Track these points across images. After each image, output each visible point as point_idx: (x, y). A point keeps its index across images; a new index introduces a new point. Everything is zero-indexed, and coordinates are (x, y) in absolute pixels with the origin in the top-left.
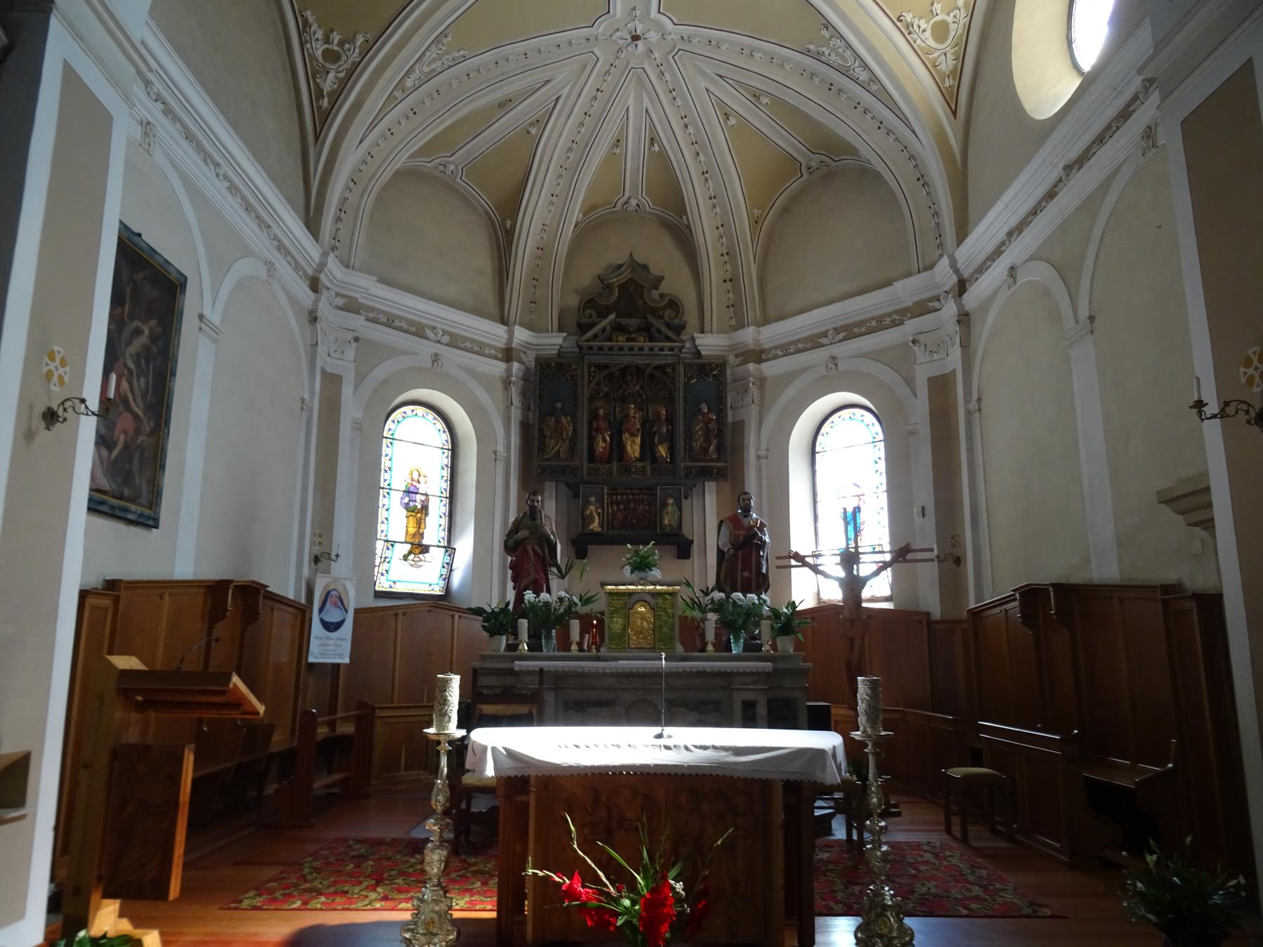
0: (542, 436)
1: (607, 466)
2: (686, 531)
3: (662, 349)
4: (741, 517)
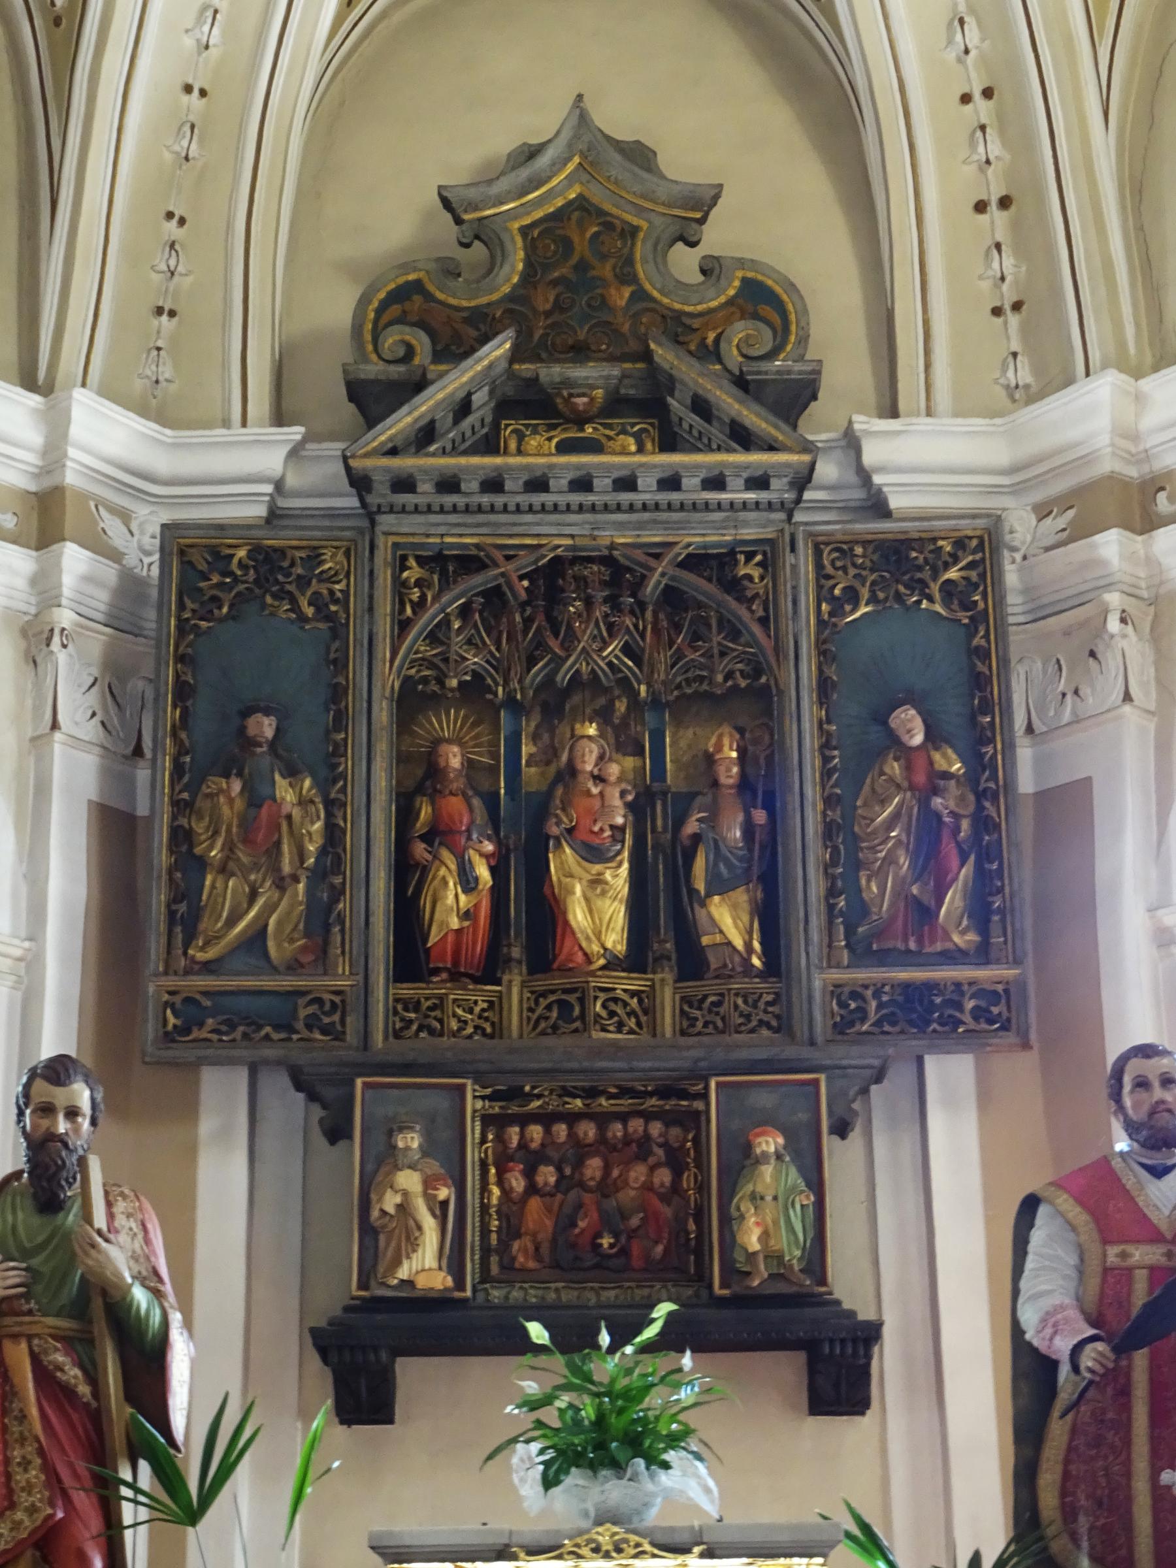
0: (188, 861)
1: (480, 996)
2: (848, 1286)
3: (716, 483)
4: (1133, 1177)
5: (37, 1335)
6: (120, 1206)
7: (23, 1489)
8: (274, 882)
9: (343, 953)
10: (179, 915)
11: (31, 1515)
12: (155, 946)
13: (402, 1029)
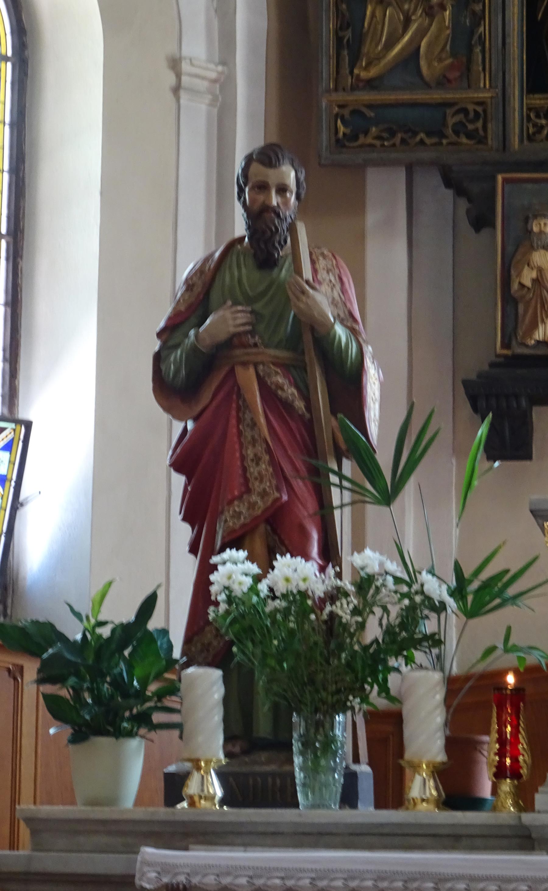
5: (263, 363)
6: (322, 264)
7: (256, 479)
8: (424, 10)
9: (484, 69)
10: (345, 40)
11: (262, 498)
12: (326, 68)
13: (534, 134)
